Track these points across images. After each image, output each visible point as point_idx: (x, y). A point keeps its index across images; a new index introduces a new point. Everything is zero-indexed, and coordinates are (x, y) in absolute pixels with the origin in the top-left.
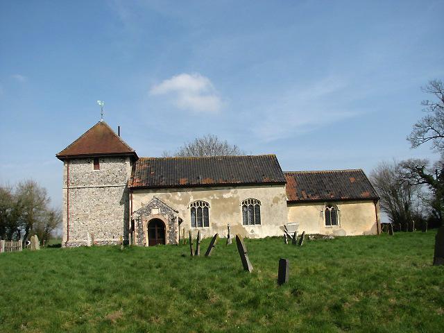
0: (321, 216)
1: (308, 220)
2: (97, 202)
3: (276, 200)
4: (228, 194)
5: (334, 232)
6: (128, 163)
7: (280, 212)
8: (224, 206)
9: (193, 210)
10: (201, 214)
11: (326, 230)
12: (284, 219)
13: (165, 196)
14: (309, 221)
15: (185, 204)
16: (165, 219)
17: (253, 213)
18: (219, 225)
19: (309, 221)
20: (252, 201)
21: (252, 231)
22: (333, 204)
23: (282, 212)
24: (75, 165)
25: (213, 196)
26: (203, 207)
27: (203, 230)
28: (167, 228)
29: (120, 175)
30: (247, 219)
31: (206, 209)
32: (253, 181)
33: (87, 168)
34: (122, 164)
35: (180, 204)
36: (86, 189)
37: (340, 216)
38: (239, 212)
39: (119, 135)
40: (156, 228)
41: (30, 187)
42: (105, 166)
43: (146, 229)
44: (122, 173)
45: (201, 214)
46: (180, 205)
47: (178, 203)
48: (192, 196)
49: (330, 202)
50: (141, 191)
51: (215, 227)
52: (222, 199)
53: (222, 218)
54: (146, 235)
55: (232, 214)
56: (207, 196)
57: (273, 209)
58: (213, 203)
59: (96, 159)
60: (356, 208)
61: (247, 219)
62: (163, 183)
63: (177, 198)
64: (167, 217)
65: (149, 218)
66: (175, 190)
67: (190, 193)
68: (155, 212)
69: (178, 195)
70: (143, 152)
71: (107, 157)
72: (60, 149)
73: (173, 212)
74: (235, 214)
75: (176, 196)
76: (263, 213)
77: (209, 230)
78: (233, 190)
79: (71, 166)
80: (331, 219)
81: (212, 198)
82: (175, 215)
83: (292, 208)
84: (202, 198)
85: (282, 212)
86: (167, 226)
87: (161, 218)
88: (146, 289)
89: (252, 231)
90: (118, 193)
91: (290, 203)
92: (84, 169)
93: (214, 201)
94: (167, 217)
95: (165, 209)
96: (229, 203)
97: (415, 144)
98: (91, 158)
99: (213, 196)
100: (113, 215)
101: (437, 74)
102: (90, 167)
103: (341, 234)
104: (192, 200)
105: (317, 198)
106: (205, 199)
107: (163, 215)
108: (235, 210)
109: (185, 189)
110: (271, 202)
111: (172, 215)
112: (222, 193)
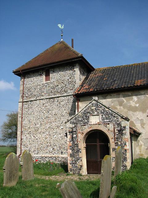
1: (84, 152)
2: (46, 115)
6: (77, 70)
13: (117, 102)
16: (109, 130)
28: (112, 145)
29: (70, 83)
33: (40, 80)
34: (71, 72)
36: (38, 101)
39: (73, 47)
40: (98, 144)
42: (55, 76)
43: (82, 145)
44: (73, 83)
46: (138, 112)
47: (135, 109)
54: (83, 155)
62: (115, 86)
63: (133, 104)
64: (111, 126)
65: (87, 129)
66: (130, 93)
68: (94, 120)
70: (98, 63)
73: (120, 119)
75: (131, 102)
79: (27, 80)
82: (124, 123)
90: (67, 102)
92: (37, 81)
94: (111, 126)
95: (109, 115)
101: (103, 194)
107: (106, 124)
111: (119, 125)
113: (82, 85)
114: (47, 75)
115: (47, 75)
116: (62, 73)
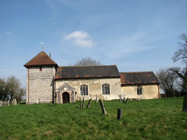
1: (130, 92)
2: (41, 85)
6: (54, 68)
8: (94, 87)
9: (81, 88)
10: (85, 90)
12: (120, 92)
13: (69, 82)
15: (78, 86)
16: (70, 92)
18: (92, 94)
19: (130, 93)
20: (106, 84)
24: (32, 70)
25: (90, 82)
26: (85, 87)
27: (85, 97)
28: (70, 96)
29: (51, 73)
30: (104, 92)
31: (87, 88)
32: (107, 76)
33: (37, 71)
34: (51, 69)
35: (76, 86)
36: (36, 80)
38: (101, 89)
39: (50, 57)
40: (66, 96)
42: (44, 70)
43: (61, 96)
44: (51, 73)
45: (85, 90)
46: (76, 86)
47: (75, 85)
48: (81, 83)
50: (59, 80)
51: (91, 95)
52: (93, 84)
53: (93, 92)
54: (62, 99)
56: (87, 83)
58: (90, 85)
59: (41, 67)
61: (104, 92)
62: (69, 77)
63: (75, 83)
64: (70, 91)
65: (63, 92)
66: (74, 80)
67: (80, 81)
68: (65, 89)
69: (75, 82)
70: (60, 64)
71: (45, 66)
72: (25, 63)
73: (73, 89)
75: (74, 83)
77: (88, 97)
79: (30, 70)
80: (139, 92)
82: (74, 90)
86: (70, 95)
87: (68, 92)
90: (50, 81)
91: (122, 85)
92: (35, 71)
93: (90, 84)
94: (70, 91)
95: (70, 88)
96: (97, 85)
97: (175, 60)
98: (38, 66)
99: (90, 82)
100: (48, 90)
101: (184, 31)
102: (38, 70)
104: (81, 84)
106: (86, 84)
107: (69, 90)
109: (78, 80)
110: (114, 85)
111: (73, 91)
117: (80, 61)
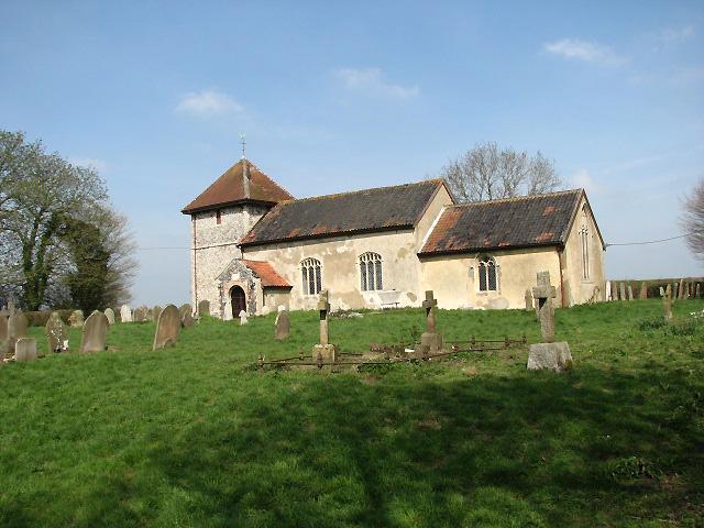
0: (471, 275)
3: (402, 253)
4: (343, 246)
5: (490, 301)
7: (407, 272)
10: (372, 269)
11: (478, 299)
14: (456, 287)
16: (244, 286)
17: (372, 269)
19: (456, 287)
21: (372, 300)
22: (489, 255)
23: (410, 270)
25: (325, 250)
26: (374, 261)
28: (247, 299)
35: (286, 262)
37: (500, 275)
38: (354, 272)
41: (124, 219)
42: (227, 218)
47: (288, 262)
48: (303, 251)
49: (485, 253)
52: (336, 255)
55: (346, 275)
56: (319, 252)
57: (397, 267)
60: (526, 261)
64: (246, 283)
66: (285, 245)
69: (288, 252)
74: (350, 275)
76: (531, 260)
78: (348, 241)
80: (488, 280)
81: (324, 253)
83: (430, 265)
84: (313, 254)
85: (410, 270)
88: (572, 469)
89: (372, 300)
92: (208, 223)
93: (327, 258)
99: (325, 250)
103: (500, 306)
105: (463, 246)
106: (316, 257)
108: (351, 270)
112: (334, 246)
113: (250, 232)
114: (218, 217)
115: (218, 217)
116: (234, 215)
117: (131, 279)
